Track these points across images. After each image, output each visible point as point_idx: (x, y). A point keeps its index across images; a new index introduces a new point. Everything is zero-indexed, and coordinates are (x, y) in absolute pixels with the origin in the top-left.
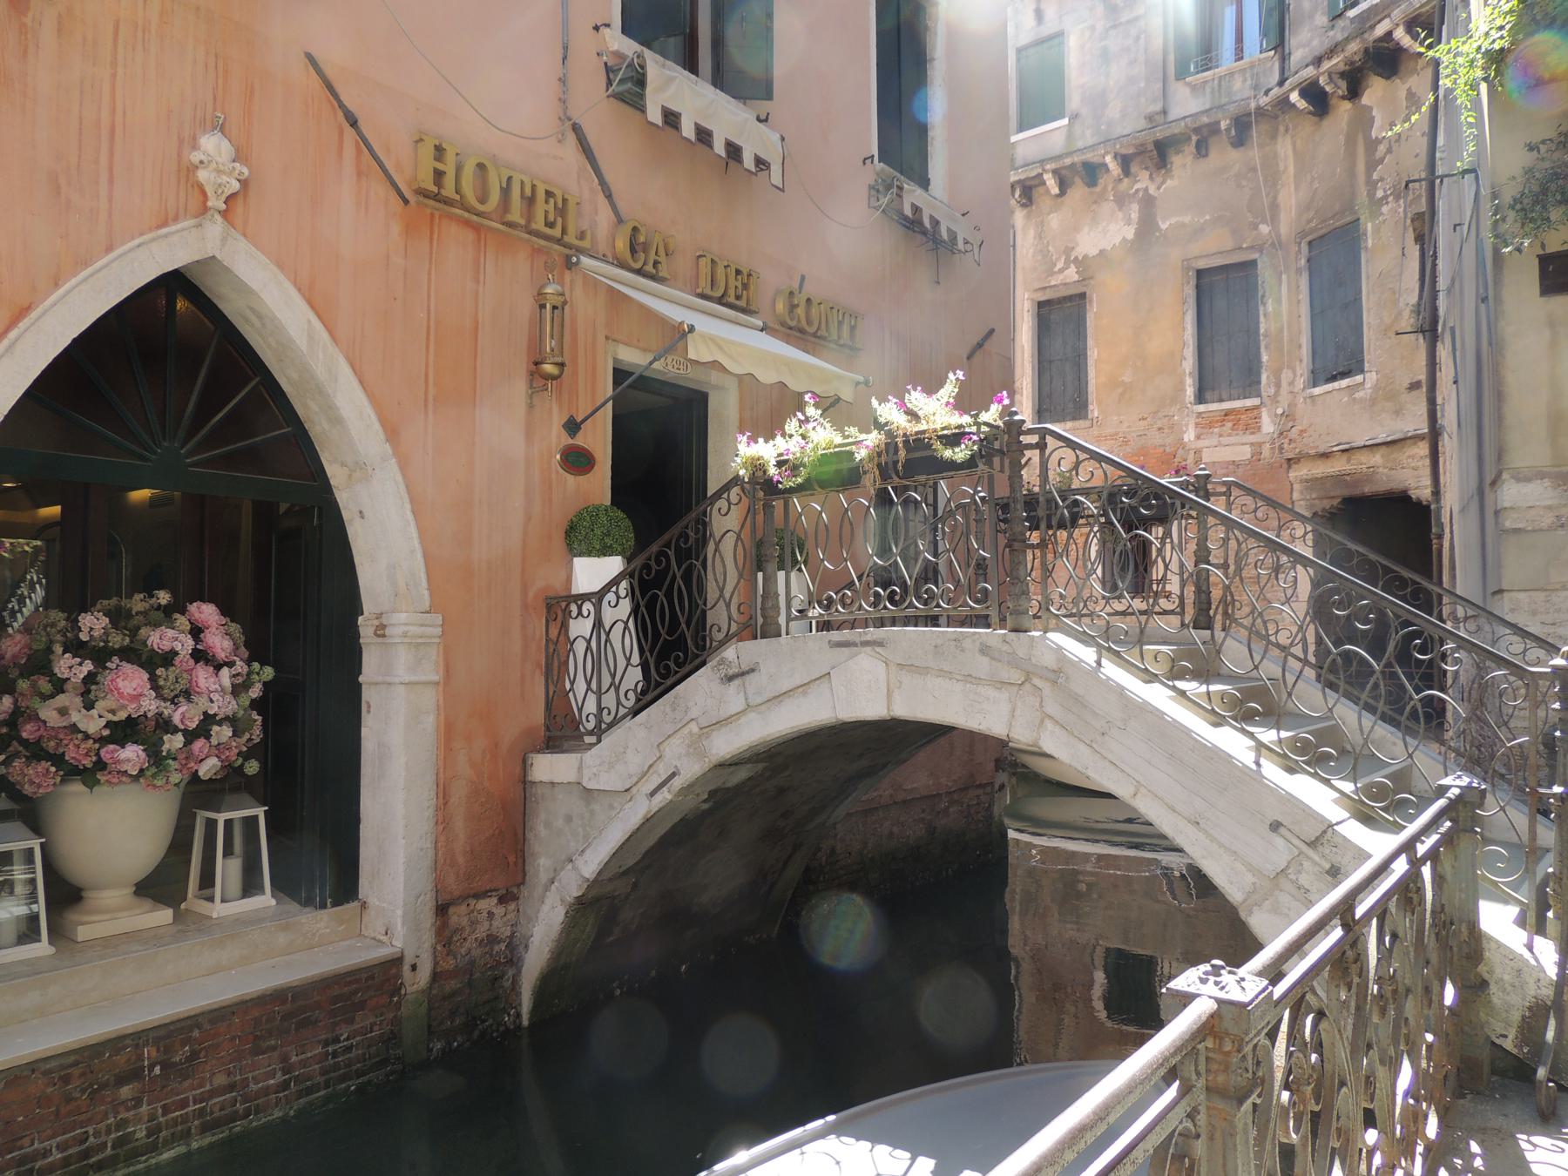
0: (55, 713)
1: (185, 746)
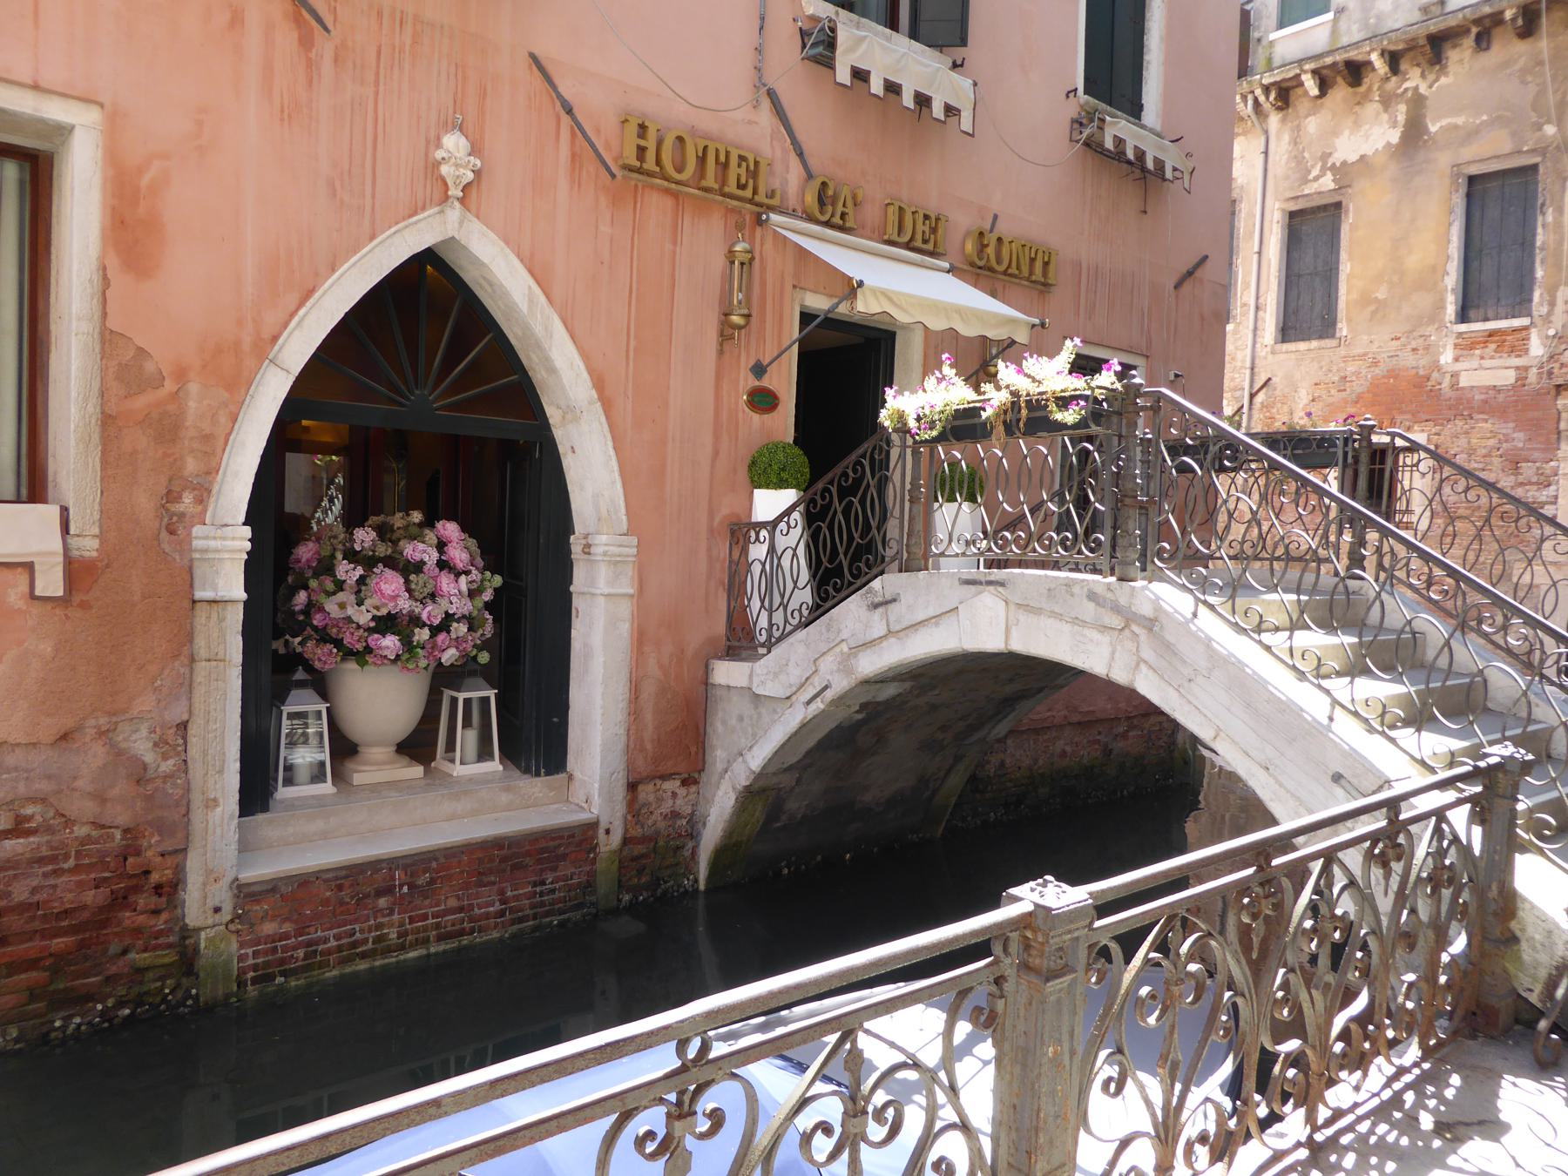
0: (336, 606)
1: (431, 637)
